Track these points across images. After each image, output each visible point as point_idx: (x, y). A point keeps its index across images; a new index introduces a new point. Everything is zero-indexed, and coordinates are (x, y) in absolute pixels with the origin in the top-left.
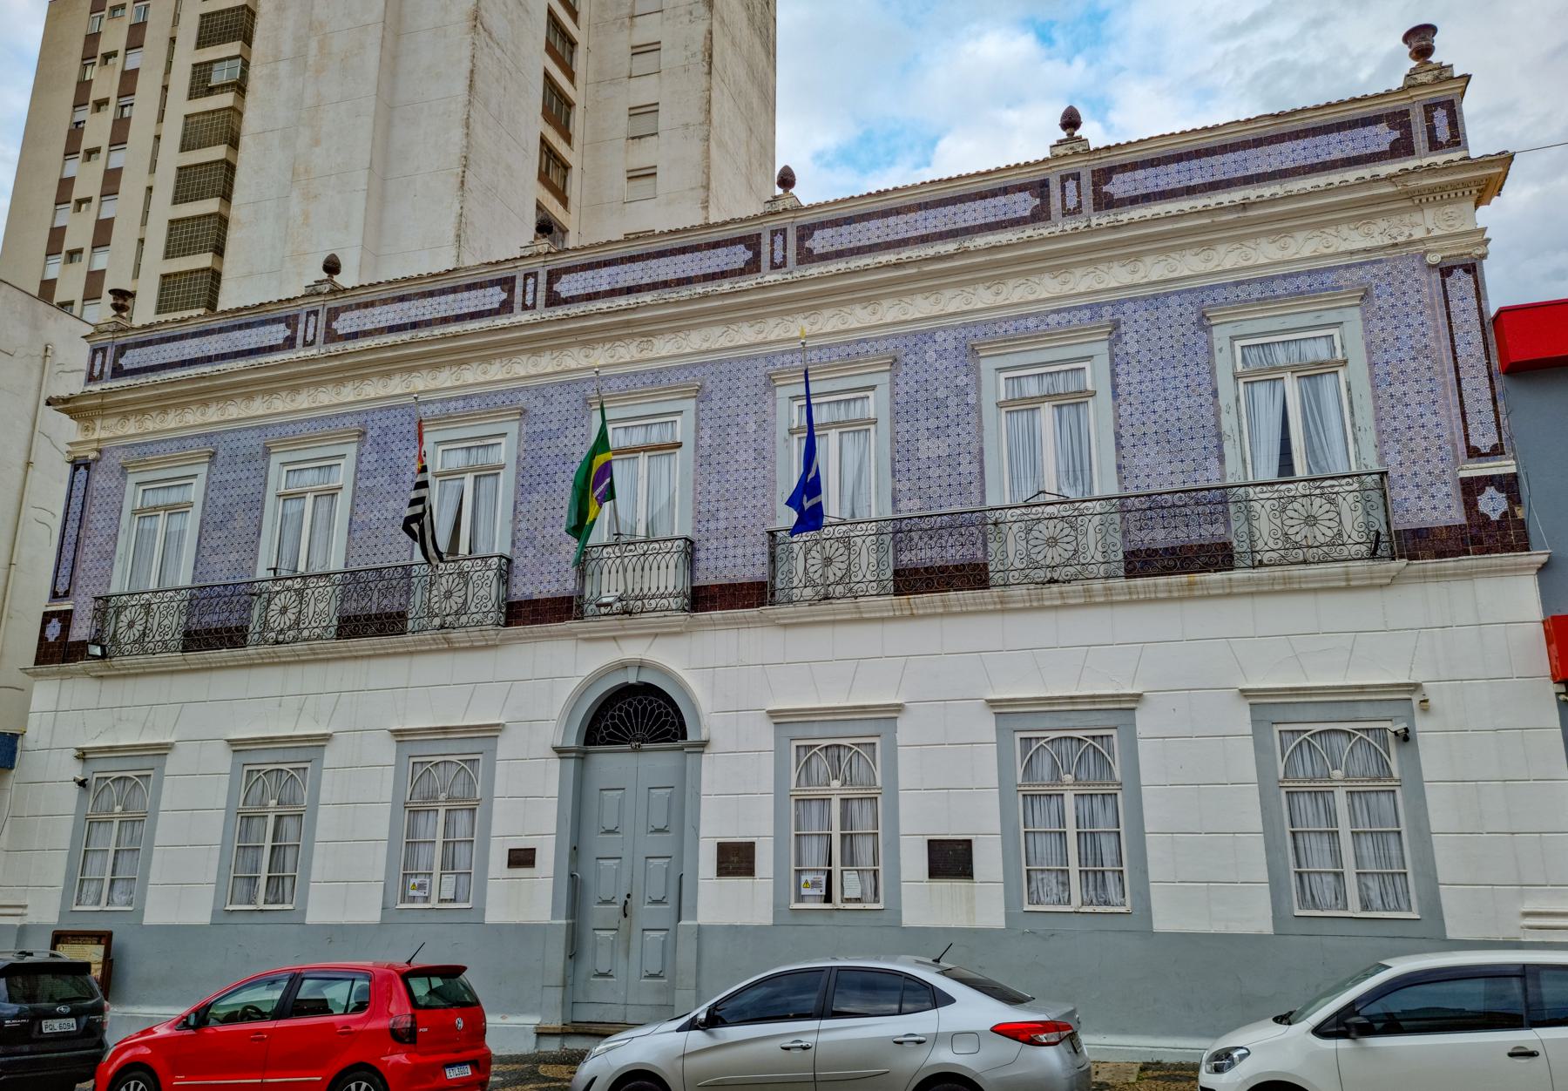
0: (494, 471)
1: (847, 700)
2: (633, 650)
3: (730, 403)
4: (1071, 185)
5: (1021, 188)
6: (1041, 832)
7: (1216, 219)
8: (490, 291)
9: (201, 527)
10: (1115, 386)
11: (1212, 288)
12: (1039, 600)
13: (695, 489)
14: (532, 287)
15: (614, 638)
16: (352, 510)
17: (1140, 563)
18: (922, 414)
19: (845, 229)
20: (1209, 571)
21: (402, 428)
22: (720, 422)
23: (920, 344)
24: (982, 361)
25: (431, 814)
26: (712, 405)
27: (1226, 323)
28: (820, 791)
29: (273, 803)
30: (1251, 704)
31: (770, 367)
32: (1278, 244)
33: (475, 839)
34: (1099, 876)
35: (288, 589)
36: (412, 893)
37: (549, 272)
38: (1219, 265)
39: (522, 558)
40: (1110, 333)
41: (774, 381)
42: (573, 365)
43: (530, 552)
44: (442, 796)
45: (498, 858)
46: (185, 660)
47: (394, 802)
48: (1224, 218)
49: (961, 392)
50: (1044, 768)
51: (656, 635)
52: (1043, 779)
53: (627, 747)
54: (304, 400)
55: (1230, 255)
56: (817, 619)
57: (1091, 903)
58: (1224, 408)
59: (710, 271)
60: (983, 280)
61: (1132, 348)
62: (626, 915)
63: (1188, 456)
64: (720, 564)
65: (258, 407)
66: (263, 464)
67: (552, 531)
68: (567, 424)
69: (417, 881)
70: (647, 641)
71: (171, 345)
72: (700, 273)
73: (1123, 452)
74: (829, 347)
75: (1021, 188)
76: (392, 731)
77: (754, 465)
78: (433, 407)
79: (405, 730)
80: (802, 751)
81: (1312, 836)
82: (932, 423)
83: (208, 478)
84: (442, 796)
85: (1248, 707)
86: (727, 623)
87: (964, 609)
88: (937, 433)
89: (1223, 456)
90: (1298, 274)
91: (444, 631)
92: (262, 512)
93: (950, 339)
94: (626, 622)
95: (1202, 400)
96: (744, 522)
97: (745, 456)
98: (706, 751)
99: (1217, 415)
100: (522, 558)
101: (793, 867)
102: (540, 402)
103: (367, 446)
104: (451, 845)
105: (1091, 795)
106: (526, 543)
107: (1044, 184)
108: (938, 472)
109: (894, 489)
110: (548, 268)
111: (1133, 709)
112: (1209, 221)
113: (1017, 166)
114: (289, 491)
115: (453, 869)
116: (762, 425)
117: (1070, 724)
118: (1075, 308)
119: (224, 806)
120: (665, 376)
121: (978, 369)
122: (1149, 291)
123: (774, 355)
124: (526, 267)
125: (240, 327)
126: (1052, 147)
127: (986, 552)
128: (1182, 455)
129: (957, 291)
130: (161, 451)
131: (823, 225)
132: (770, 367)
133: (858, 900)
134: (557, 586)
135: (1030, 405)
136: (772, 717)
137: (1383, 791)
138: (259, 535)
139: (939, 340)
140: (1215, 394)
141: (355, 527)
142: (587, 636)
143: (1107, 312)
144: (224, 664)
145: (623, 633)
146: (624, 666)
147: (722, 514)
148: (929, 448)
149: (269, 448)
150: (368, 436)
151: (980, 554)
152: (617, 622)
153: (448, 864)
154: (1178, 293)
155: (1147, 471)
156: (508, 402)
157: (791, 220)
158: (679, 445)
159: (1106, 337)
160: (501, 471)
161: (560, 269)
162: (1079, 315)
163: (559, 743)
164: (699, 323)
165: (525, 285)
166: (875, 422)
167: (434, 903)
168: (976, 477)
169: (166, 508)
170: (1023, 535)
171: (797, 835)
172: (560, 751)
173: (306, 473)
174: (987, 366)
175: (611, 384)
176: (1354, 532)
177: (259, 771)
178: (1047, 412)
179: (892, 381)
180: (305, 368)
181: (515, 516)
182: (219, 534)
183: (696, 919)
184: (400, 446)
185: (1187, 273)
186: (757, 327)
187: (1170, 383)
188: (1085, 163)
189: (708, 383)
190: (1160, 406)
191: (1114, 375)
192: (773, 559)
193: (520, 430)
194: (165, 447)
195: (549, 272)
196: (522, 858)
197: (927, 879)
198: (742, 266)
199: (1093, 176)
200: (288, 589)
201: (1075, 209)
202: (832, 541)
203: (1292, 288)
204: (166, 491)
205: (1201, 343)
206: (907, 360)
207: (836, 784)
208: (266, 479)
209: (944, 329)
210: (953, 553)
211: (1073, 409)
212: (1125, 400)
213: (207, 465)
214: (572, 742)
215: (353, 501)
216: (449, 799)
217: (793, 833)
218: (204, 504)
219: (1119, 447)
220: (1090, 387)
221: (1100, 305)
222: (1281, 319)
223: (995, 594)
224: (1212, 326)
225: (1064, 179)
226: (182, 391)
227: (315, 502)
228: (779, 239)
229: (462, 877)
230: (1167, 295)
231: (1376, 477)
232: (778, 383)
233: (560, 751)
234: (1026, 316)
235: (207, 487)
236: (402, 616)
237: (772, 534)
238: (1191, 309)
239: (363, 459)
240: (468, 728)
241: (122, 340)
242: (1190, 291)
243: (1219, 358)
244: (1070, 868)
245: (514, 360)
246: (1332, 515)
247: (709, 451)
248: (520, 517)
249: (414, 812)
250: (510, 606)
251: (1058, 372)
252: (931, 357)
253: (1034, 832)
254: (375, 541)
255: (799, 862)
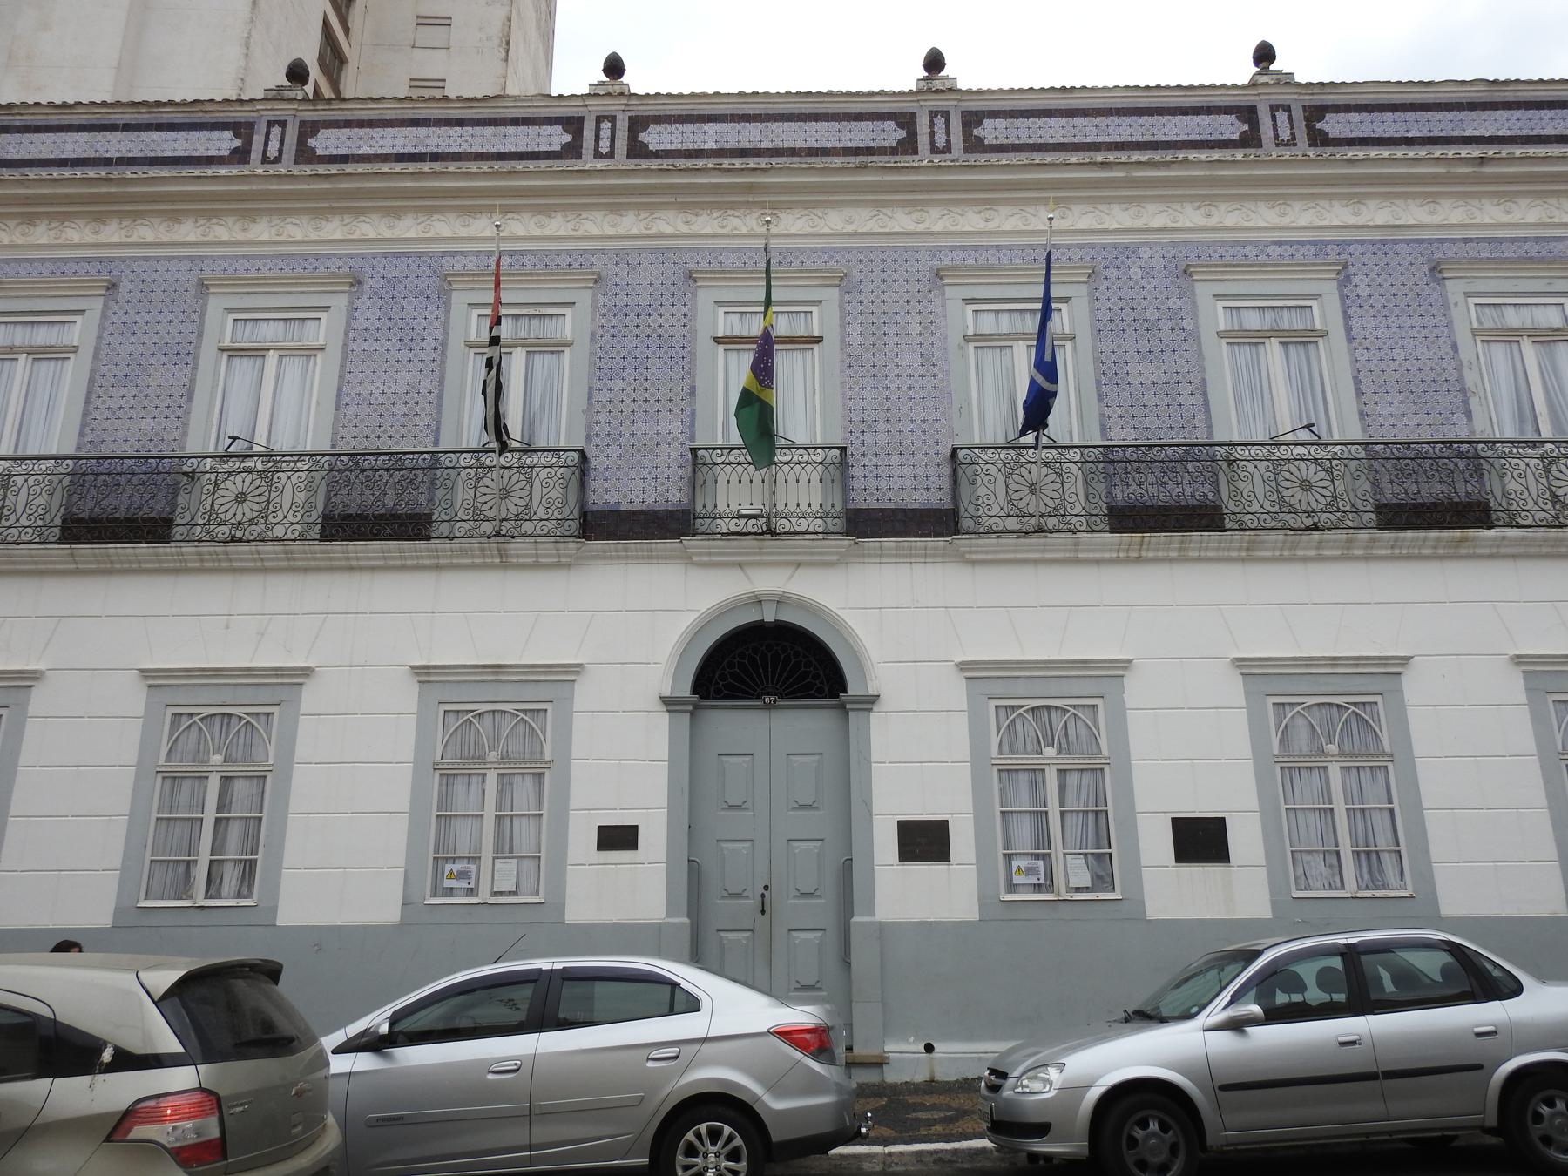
0: (557, 346)
1: (251, 661)
2: (768, 581)
3: (885, 297)
4: (1282, 116)
5: (1227, 110)
6: (1072, 811)
7: (1453, 170)
8: (547, 129)
9: (92, 381)
10: (1348, 329)
11: (1442, 241)
12: (1291, 548)
13: (843, 394)
14: (609, 133)
15: (740, 565)
16: (341, 377)
17: (1396, 516)
18: (1130, 334)
19: (1022, 122)
20: (1482, 528)
21: (419, 282)
22: (872, 318)
23: (1122, 258)
24: (1197, 285)
25: (475, 779)
26: (862, 297)
27: (255, 293)
28: (1032, 760)
29: (217, 759)
30: (1524, 672)
31: (936, 263)
32: (1202, 210)
33: (544, 812)
34: (1374, 857)
35: (248, 471)
36: (448, 883)
37: (630, 118)
38: (1522, 219)
39: (602, 458)
40: (1338, 273)
41: (450, 282)
42: (669, 230)
43: (614, 452)
44: (493, 756)
45: (582, 839)
46: (72, 555)
47: (417, 762)
48: (1461, 170)
49: (1176, 315)
50: (1301, 737)
51: (799, 565)
52: (1301, 750)
53: (758, 702)
54: (262, 230)
55: (798, 221)
56: (1019, 556)
57: (1367, 888)
58: (1465, 363)
59: (850, 145)
60: (1192, 198)
61: (1364, 291)
62: (763, 912)
63: (1433, 408)
64: (883, 484)
65: (188, 231)
66: (197, 307)
67: (644, 428)
68: (663, 300)
69: (456, 867)
70: (788, 571)
71: (43, 136)
72: (838, 145)
73: (1364, 398)
74: (1010, 248)
75: (1227, 110)
76: (412, 667)
77: (921, 372)
78: (464, 261)
79: (435, 667)
80: (1002, 713)
81: (1299, 814)
82: (1143, 346)
83: (104, 316)
84: (493, 756)
85: (1521, 675)
86: (898, 555)
87: (1203, 554)
88: (1149, 357)
89: (1470, 412)
90: (1526, 240)
91: (502, 540)
92: (195, 368)
93: (1158, 256)
94: (973, 541)
95: (1442, 353)
96: (911, 437)
97: (908, 361)
98: (875, 709)
99: (1459, 368)
100: (602, 458)
101: (1001, 851)
102: (622, 270)
103: (365, 298)
104: (508, 821)
105: (1358, 767)
106: (607, 440)
107: (581, 120)
108: (1155, 400)
109: (1102, 415)
110: (629, 114)
111: (574, 681)
112: (1444, 171)
113: (1224, 86)
114: (237, 346)
115: (511, 851)
116: (928, 326)
117: (1330, 689)
118: (1298, 242)
119: (134, 760)
120: (797, 257)
121: (1194, 294)
122: (1377, 235)
123: (940, 249)
124: (598, 107)
125: (159, 127)
126: (918, 80)
127: (431, 500)
128: (1428, 407)
129: (1162, 207)
130: (24, 273)
131: (994, 114)
132: (936, 263)
133: (510, 893)
134: (654, 496)
135: (1256, 339)
136: (146, 678)
137: (1087, 770)
138: (190, 399)
139: (1146, 256)
140: (1455, 347)
141: (346, 399)
142: (706, 559)
143: (1333, 252)
144: (135, 566)
145: (757, 558)
146: (758, 601)
147: (881, 426)
148: (1142, 374)
149: (207, 287)
150: (365, 287)
151: (423, 500)
152: (194, 549)
153: (504, 845)
154: (1408, 242)
155: (1392, 420)
156: (576, 265)
157: (955, 103)
158: (819, 340)
159: (1334, 276)
160: (567, 350)
161: (648, 117)
162: (1303, 250)
163: (667, 693)
164: (843, 201)
165: (598, 130)
166: (1073, 338)
167: (484, 896)
168: (1199, 410)
169: (31, 351)
170: (211, 488)
171: (1002, 812)
172: (669, 703)
173: (264, 325)
174: (1203, 291)
175: (722, 258)
176: (1231, 502)
177: (191, 715)
178: (1274, 348)
179: (1090, 294)
180: (274, 187)
181: (590, 404)
182: (123, 391)
183: (873, 914)
184: (415, 302)
185: (1412, 222)
186: (916, 215)
187: (1407, 332)
188: (1296, 97)
189: (855, 272)
190: (1399, 354)
191: (1347, 317)
192: (693, 484)
193: (595, 301)
194: (30, 268)
195: (630, 118)
196: (618, 838)
197: (1174, 864)
198: (894, 144)
199: (1305, 111)
200: (248, 471)
201: (1288, 140)
202: (512, 472)
203: (1521, 252)
204: (29, 328)
205: (1435, 295)
206: (1107, 273)
207: (1050, 751)
208: (202, 324)
209: (1150, 245)
210: (1183, 490)
211: (1301, 349)
212: (1360, 344)
213: (101, 299)
214: (685, 690)
215: (343, 366)
216: (504, 759)
217: (998, 809)
218: (97, 349)
219: (1359, 393)
220: (1318, 326)
221: (1326, 243)
222: (1515, 282)
223: (1247, 538)
224: (1444, 278)
225: (599, 120)
226: (67, 196)
227: (280, 364)
228: (606, 125)
229: (526, 863)
230: (1395, 242)
231: (837, 452)
232: (211, 290)
233: (669, 703)
234: (1244, 244)
235: (102, 328)
236: (168, 522)
237: (694, 450)
238: (1421, 259)
239: (357, 314)
240: (532, 669)
241: (310, 116)
242: (1420, 241)
243: (1455, 312)
244: (483, 855)
245: (584, 216)
246: (1015, 487)
247: (859, 351)
248: (598, 407)
249: (448, 776)
250: (584, 515)
251: (1282, 308)
252: (1135, 273)
253: (1295, 809)
254: (379, 420)
255: (1007, 845)
